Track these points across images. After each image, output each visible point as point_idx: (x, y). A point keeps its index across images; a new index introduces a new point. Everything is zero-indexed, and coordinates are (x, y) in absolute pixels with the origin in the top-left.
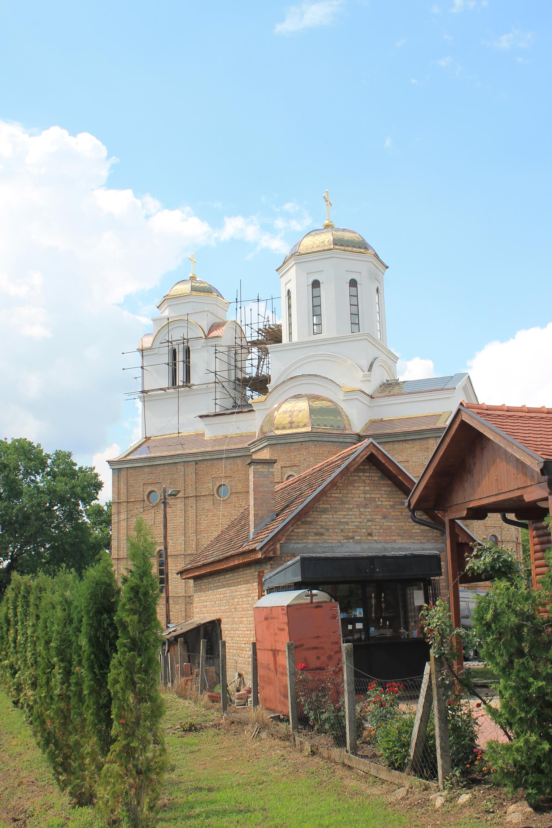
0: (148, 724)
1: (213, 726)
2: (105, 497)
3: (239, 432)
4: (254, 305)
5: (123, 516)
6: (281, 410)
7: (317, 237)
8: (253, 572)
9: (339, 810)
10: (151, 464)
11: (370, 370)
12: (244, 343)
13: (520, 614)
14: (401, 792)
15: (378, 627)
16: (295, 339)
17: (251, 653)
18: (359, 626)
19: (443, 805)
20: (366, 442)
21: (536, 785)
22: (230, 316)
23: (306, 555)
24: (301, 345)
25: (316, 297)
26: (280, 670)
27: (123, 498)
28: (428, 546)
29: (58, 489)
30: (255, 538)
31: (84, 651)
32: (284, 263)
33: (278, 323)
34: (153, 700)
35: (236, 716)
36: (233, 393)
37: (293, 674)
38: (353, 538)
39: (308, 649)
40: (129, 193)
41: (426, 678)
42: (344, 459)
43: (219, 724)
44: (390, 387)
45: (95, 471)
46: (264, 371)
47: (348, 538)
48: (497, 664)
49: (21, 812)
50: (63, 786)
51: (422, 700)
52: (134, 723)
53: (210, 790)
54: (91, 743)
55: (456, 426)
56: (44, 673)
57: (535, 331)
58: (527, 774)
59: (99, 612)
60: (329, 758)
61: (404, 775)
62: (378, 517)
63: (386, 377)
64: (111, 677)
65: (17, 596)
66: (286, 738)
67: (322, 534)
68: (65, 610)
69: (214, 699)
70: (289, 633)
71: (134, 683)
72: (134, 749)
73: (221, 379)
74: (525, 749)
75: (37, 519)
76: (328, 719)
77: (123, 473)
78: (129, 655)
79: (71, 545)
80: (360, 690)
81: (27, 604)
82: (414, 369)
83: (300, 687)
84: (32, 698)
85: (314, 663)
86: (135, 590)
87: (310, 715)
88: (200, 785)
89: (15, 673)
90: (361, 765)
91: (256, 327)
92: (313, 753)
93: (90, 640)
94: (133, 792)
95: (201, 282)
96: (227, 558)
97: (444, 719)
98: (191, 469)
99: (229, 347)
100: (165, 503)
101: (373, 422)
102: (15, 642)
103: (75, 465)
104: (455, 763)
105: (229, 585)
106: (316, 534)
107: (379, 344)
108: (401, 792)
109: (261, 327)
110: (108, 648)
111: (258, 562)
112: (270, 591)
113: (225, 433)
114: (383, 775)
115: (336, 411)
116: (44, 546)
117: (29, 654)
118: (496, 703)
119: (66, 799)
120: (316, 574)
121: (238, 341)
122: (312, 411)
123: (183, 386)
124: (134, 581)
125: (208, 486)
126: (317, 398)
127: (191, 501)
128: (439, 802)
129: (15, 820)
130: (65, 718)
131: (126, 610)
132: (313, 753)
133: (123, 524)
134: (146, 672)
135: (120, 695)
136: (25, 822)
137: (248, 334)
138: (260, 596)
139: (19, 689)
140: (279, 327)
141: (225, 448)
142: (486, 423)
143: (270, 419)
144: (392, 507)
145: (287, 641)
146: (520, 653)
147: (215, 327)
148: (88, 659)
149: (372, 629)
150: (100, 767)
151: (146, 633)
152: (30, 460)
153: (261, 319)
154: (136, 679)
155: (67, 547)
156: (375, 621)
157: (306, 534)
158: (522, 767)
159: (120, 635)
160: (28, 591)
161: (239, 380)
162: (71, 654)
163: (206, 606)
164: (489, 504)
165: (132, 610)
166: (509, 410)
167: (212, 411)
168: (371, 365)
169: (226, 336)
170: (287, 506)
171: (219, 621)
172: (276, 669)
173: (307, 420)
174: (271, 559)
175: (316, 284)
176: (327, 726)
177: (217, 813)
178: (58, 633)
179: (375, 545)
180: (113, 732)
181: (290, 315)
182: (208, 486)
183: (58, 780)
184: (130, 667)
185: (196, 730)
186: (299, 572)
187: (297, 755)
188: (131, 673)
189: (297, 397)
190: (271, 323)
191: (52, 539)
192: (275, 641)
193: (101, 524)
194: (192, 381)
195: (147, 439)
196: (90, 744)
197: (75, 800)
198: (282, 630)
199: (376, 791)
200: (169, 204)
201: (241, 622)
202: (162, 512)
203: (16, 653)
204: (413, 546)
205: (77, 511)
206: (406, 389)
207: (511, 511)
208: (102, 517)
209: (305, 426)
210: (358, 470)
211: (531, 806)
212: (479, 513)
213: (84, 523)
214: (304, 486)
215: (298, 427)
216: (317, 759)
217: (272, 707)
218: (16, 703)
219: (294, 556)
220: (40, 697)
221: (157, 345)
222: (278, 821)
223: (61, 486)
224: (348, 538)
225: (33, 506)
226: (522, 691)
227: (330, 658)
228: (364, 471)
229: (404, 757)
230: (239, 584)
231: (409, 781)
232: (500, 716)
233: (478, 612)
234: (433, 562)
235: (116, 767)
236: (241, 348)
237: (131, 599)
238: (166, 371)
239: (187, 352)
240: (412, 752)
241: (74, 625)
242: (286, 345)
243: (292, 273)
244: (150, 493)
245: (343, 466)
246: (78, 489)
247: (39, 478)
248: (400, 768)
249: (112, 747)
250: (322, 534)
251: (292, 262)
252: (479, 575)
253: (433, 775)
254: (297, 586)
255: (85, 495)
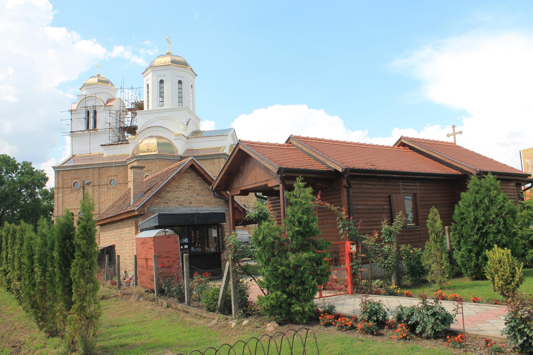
0: (91, 294)
1: (114, 296)
2: (50, 185)
3: (121, 153)
4: (130, 91)
5: (60, 195)
6: (143, 143)
7: (163, 59)
8: (133, 221)
9: (185, 332)
10: (75, 169)
11: (187, 125)
12: (124, 110)
13: (275, 238)
14: (214, 322)
15: (195, 248)
16: (150, 108)
17: (134, 260)
18: (186, 247)
19: (235, 326)
20: (190, 159)
21: (280, 314)
22: (118, 95)
23: (160, 213)
24: (153, 112)
25: (161, 88)
26: (150, 268)
27: (61, 186)
28: (218, 208)
29: (25, 181)
30: (133, 205)
31: (56, 259)
32: (146, 70)
33: (142, 100)
34: (93, 282)
35: (126, 291)
36: (118, 134)
37: (157, 269)
38: (182, 205)
39: (164, 257)
40: (64, 29)
41: (227, 268)
42: (178, 166)
43: (117, 296)
44: (197, 134)
45: (44, 172)
46: (135, 124)
47: (180, 205)
48: (262, 260)
49: (17, 343)
50: (41, 327)
51: (224, 278)
52: (84, 294)
53: (118, 326)
54: (60, 305)
55: (236, 151)
56: (27, 272)
57: (262, 110)
58: (275, 309)
59: (64, 239)
60: (176, 308)
61: (215, 314)
62: (195, 195)
63: (194, 129)
64: (72, 271)
65: (7, 234)
66: (153, 300)
67: (167, 203)
68: (42, 239)
69: (113, 284)
70: (154, 250)
71: (84, 274)
72: (85, 307)
73: (113, 127)
74: (275, 298)
75: (13, 196)
76: (175, 290)
77: (61, 173)
78: (81, 260)
79: (32, 209)
80: (191, 276)
81: (14, 238)
82: (206, 126)
83: (159, 275)
84: (19, 286)
85: (166, 264)
86: (84, 228)
87: (166, 289)
88: (113, 324)
89: (7, 274)
90: (193, 310)
91: (130, 102)
92: (168, 306)
93: (59, 254)
94: (84, 328)
95: (103, 78)
96: (119, 215)
97: (235, 287)
98: (96, 172)
99: (117, 111)
100: (83, 188)
101: (188, 150)
102: (6, 258)
103: (34, 168)
104: (241, 307)
105: (119, 228)
106: (165, 203)
107: (192, 112)
108: (214, 322)
109: (133, 101)
110: (69, 257)
111: (135, 217)
112: (142, 230)
113: (114, 154)
114: (205, 315)
115: (170, 145)
116: (16, 210)
117: (16, 264)
118: (261, 278)
119: (43, 334)
120: (165, 221)
121: (122, 108)
122: (159, 144)
123: (93, 130)
124: (83, 223)
125: (105, 180)
126: (161, 138)
127: (96, 188)
128: (233, 325)
129: (14, 347)
130: (42, 293)
131: (80, 238)
132: (168, 306)
133: (61, 199)
134: (90, 269)
135: (77, 280)
136: (20, 347)
137: (126, 105)
138: (136, 233)
139: (9, 281)
140: (142, 102)
141: (114, 161)
142: (252, 150)
143: (137, 148)
144: (202, 190)
145: (154, 254)
146: (274, 255)
147: (109, 101)
148: (59, 263)
149: (192, 248)
150: (65, 317)
151: (90, 249)
152: (9, 166)
153: (133, 98)
154: (85, 272)
155: (29, 210)
156: (196, 245)
157: (159, 203)
158: (274, 306)
159: (76, 250)
160: (15, 232)
161: (121, 128)
162: (46, 261)
163: (107, 239)
164: (251, 188)
165: (82, 238)
166: (261, 144)
167: (108, 143)
168: (188, 123)
169: (115, 105)
170: (150, 189)
171: (114, 246)
172: (147, 267)
173: (156, 148)
174: (142, 215)
175: (162, 82)
176: (175, 294)
177: (124, 336)
178: (39, 251)
179: (193, 208)
180: (73, 299)
181: (148, 96)
182: (105, 180)
183: (39, 325)
184: (82, 266)
185: (106, 298)
186: (157, 221)
187: (160, 308)
188: (82, 269)
189: (151, 137)
190: (138, 100)
191: (22, 206)
192: (147, 254)
193: (47, 199)
194: (97, 128)
195: (74, 156)
196: (59, 306)
197: (48, 335)
198: (151, 248)
199: (201, 322)
200: (85, 37)
201: (126, 246)
202: (82, 193)
203: (7, 263)
204: (212, 209)
205: (35, 192)
206: (204, 135)
207: (259, 192)
208: (49, 196)
209: (155, 151)
210: (185, 172)
211: (277, 323)
212: (245, 193)
213: (38, 198)
214: (158, 180)
215: (151, 151)
216: (170, 309)
217: (145, 286)
218: (9, 289)
219: (153, 213)
220: (25, 285)
221: (79, 108)
222: (156, 338)
223: (27, 179)
224: (180, 205)
225: (10, 189)
226: (274, 272)
227: (174, 261)
228: (188, 172)
229: (215, 305)
230: (125, 227)
231: (217, 317)
232: (264, 284)
233: (254, 236)
234: (221, 217)
235: (75, 316)
236: (122, 113)
237: (82, 232)
238: (84, 122)
239: (95, 113)
240: (219, 303)
241: (48, 247)
242: (146, 111)
243: (150, 76)
244: (75, 183)
245: (178, 170)
246: (36, 181)
247: (14, 175)
248: (213, 311)
249: (73, 306)
250: (167, 203)
251: (150, 70)
252: (252, 220)
253: (230, 313)
254: (156, 228)
255: (39, 184)
